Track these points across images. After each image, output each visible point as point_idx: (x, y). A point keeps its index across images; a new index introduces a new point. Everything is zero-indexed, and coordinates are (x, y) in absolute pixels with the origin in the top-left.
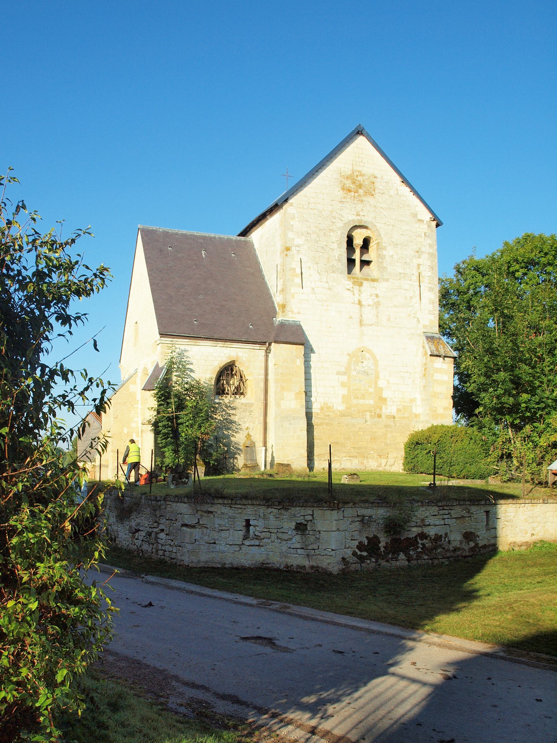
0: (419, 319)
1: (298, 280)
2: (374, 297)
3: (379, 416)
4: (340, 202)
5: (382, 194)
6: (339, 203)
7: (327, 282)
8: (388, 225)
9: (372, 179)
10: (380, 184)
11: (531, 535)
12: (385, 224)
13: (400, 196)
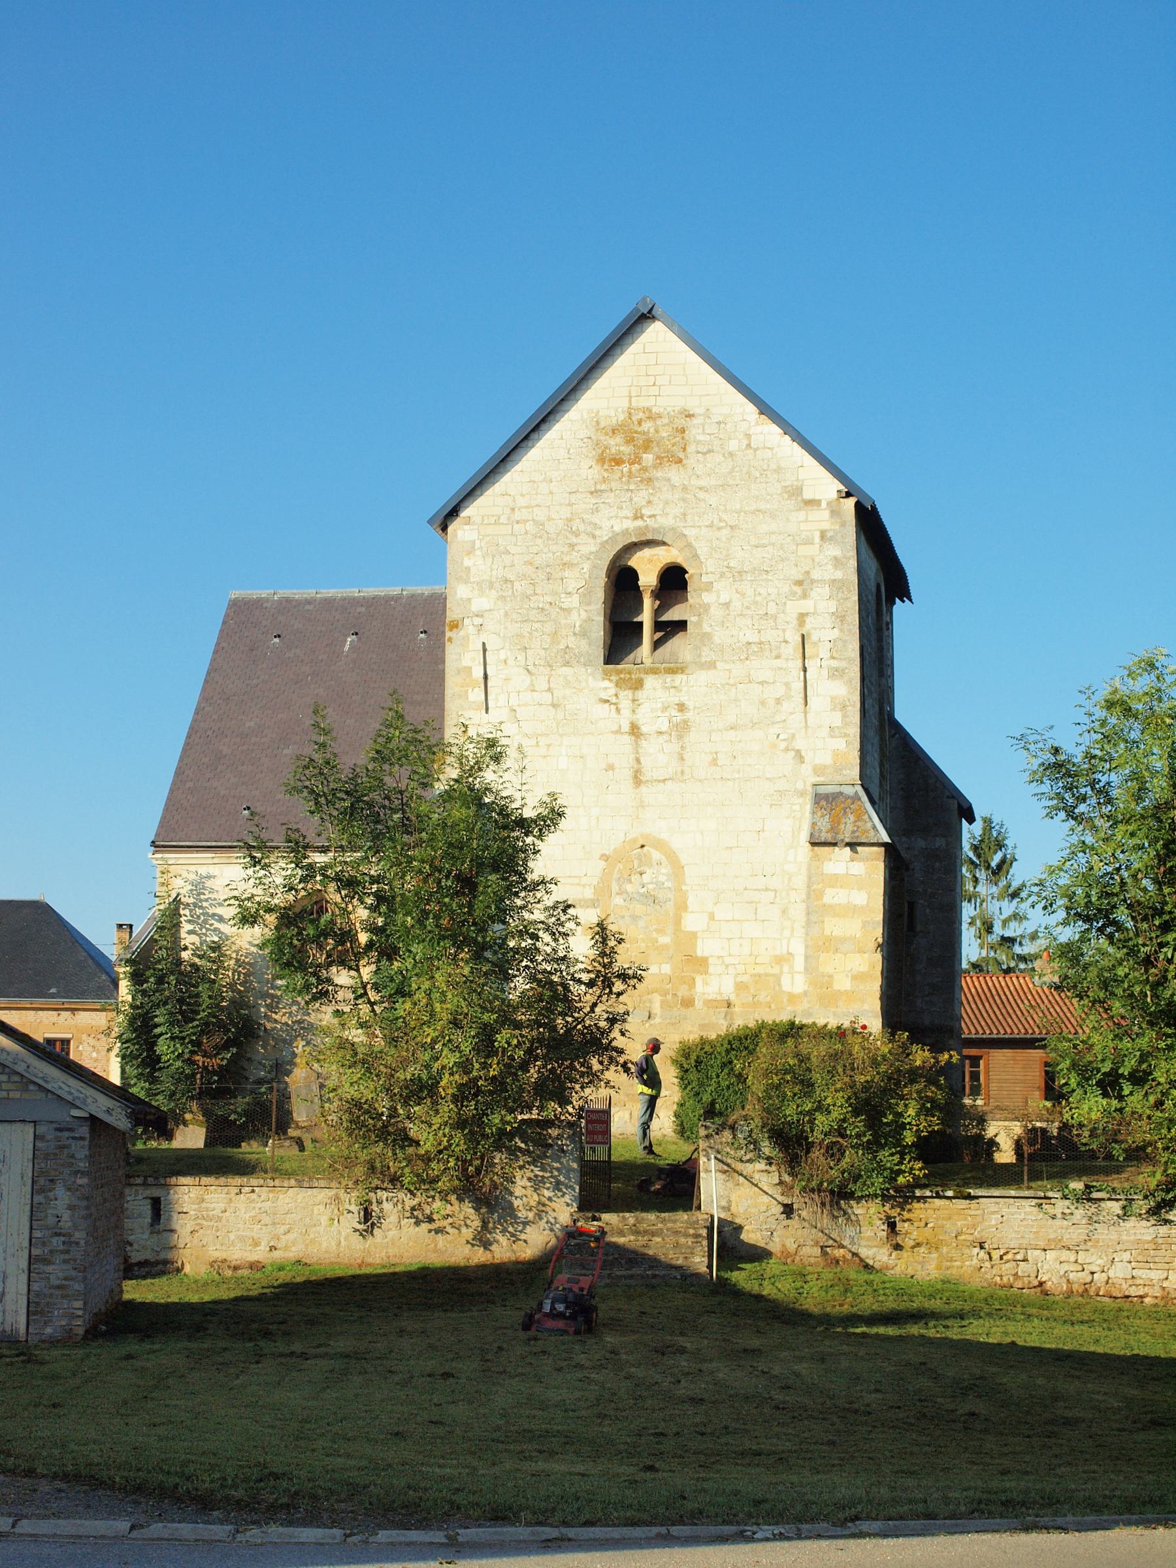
0: (803, 753)
1: (477, 695)
2: (674, 713)
3: (688, 1003)
4: (592, 493)
5: (704, 454)
6: (589, 495)
7: (549, 689)
8: (719, 529)
9: (681, 422)
10: (700, 431)
11: (268, 1249)
12: (711, 526)
13: (756, 450)
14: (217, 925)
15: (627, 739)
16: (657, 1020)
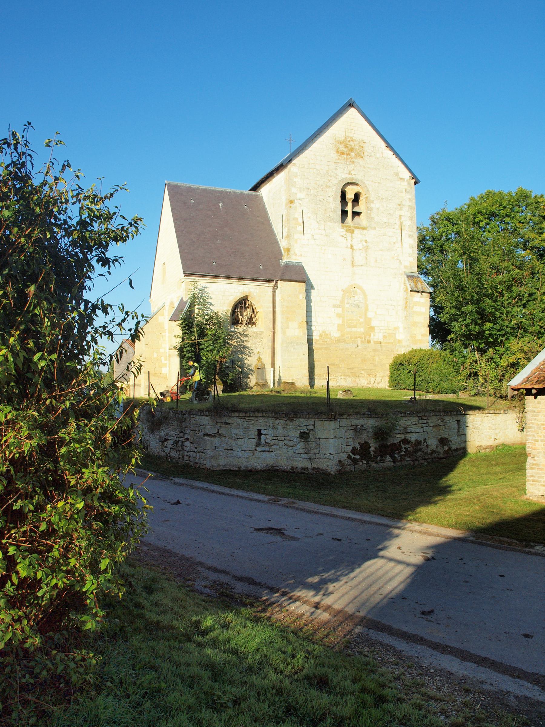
1: (300, 228)
2: (364, 243)
3: (369, 342)
9: (362, 144)
12: (372, 181)
14: (209, 306)
15: (350, 250)
16: (359, 347)
